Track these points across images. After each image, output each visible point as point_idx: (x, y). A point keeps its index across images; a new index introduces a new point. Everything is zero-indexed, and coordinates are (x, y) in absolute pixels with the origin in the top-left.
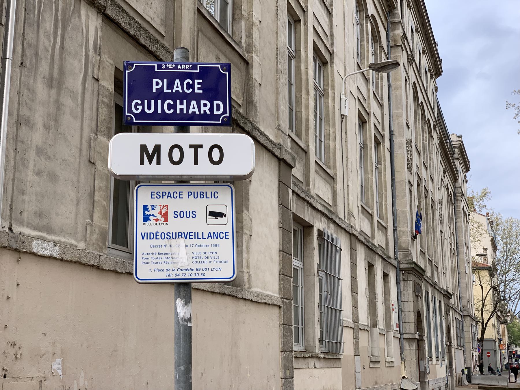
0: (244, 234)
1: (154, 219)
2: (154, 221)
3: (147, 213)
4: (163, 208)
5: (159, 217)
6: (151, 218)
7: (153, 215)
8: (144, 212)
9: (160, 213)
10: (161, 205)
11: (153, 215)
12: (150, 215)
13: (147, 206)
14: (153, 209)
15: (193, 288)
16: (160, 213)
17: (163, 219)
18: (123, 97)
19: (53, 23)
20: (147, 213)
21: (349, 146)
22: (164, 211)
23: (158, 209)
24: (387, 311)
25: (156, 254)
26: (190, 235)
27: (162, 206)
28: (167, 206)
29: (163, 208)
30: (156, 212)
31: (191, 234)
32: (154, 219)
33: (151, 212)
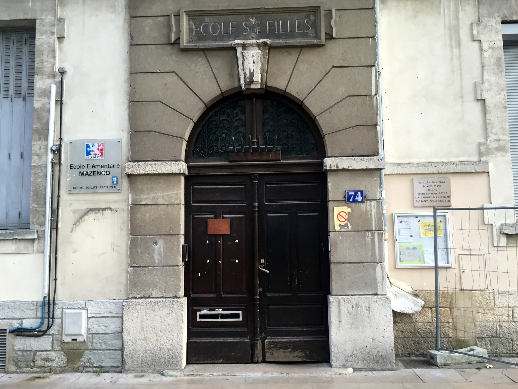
0: (300, 49)
1: (94, 154)
2: (94, 155)
3: (89, 149)
4: (100, 146)
5: (97, 152)
6: (91, 153)
7: (93, 151)
8: (87, 149)
9: (98, 149)
10: (98, 144)
11: (93, 151)
12: (91, 151)
13: (89, 144)
14: (93, 146)
15: (439, 268)
16: (98, 149)
17: (100, 154)
18: (145, 375)
19: (129, 225)
20: (89, 149)
21: (283, 14)
22: (101, 148)
23: (96, 146)
24: (45, 184)
25: (96, 187)
26: (94, 173)
27: (99, 144)
28: (103, 144)
29: (100, 146)
30: (95, 149)
31: (95, 172)
32: (94, 154)
33: (92, 149)
